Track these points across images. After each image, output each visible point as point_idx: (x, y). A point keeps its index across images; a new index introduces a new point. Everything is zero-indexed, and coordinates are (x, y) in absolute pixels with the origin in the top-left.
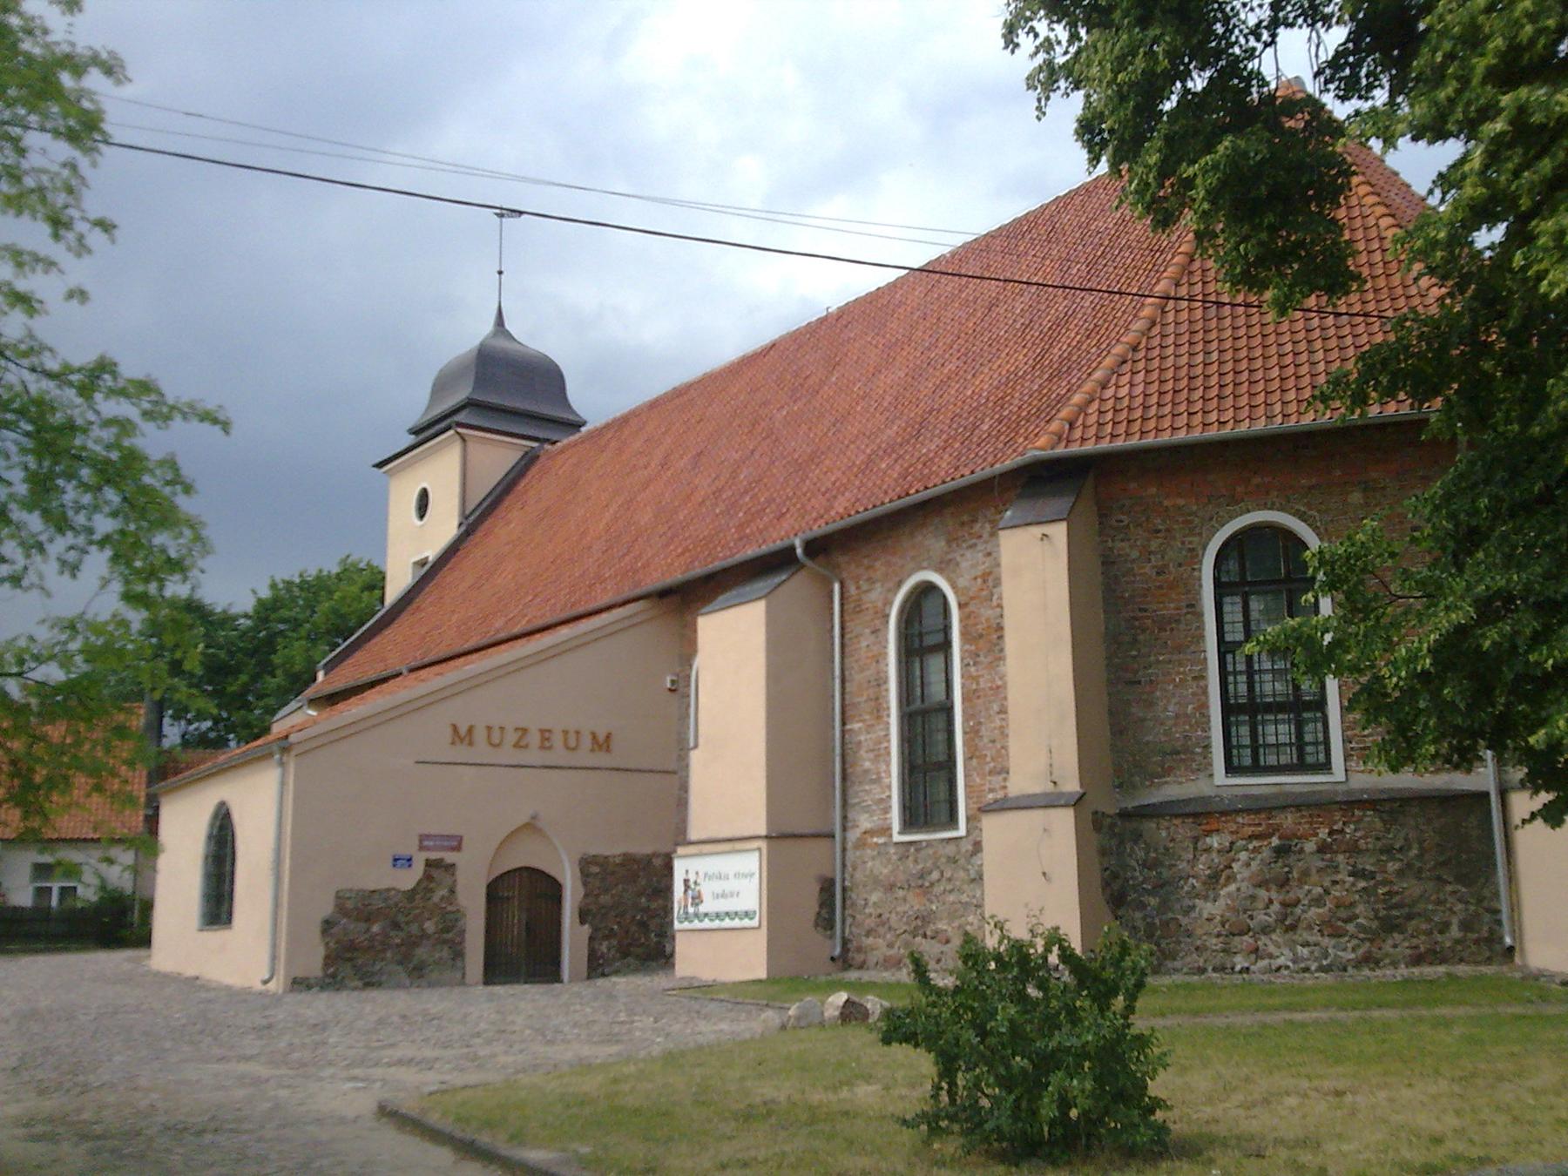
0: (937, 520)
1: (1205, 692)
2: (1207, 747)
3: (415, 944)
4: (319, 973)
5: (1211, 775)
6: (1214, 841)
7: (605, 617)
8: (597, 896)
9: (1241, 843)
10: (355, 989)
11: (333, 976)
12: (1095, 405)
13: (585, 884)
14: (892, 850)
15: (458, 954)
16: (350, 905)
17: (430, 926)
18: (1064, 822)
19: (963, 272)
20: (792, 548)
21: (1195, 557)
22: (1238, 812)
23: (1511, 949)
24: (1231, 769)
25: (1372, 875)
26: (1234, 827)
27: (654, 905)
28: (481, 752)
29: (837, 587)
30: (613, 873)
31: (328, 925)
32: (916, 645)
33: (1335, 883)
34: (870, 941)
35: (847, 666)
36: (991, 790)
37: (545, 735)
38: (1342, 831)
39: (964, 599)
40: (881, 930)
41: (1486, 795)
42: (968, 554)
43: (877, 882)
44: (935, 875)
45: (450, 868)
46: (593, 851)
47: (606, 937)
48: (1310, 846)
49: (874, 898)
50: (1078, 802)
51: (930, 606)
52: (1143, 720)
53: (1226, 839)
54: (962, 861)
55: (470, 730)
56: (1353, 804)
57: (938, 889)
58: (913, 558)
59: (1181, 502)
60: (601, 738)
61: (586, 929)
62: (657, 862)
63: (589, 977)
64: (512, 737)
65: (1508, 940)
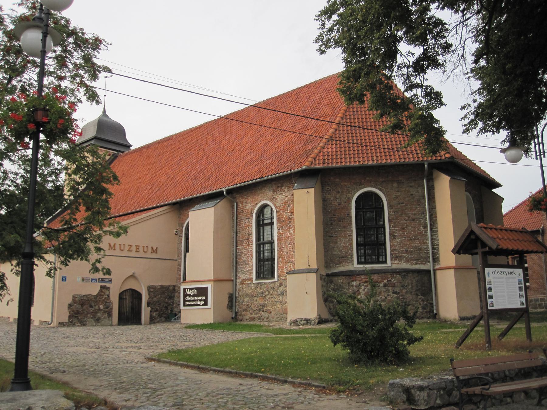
0: (270, 185)
1: (352, 240)
2: (352, 256)
3: (97, 313)
4: (67, 321)
5: (353, 264)
6: (354, 283)
7: (156, 211)
8: (153, 298)
9: (362, 284)
10: (78, 326)
11: (71, 322)
12: (322, 154)
13: (149, 295)
14: (252, 285)
15: (110, 315)
16: (77, 299)
17: (102, 307)
18: (313, 277)
19: (268, 108)
20: (223, 192)
21: (349, 200)
22: (362, 275)
23: (436, 314)
24: (359, 262)
25: (399, 293)
26: (360, 279)
27: (169, 302)
28: (117, 252)
29: (235, 204)
30: (157, 291)
31: (70, 306)
32: (262, 223)
33: (388, 295)
34: (244, 313)
35: (238, 228)
36: (286, 268)
37: (137, 247)
38: (391, 281)
39: (278, 210)
40: (248, 309)
41: (429, 271)
42: (280, 196)
43: (247, 295)
44: (267, 293)
45: (108, 289)
46: (152, 284)
47: (155, 311)
48: (382, 285)
49: (246, 300)
50: (316, 271)
51: (267, 212)
52: (334, 248)
53: (358, 283)
54: (276, 289)
55: (114, 245)
56: (394, 272)
57: (268, 297)
58: (261, 196)
59: (346, 184)
60: (155, 249)
61: (149, 309)
62: (171, 288)
63: (150, 324)
64: (127, 248)
65: (435, 311)
